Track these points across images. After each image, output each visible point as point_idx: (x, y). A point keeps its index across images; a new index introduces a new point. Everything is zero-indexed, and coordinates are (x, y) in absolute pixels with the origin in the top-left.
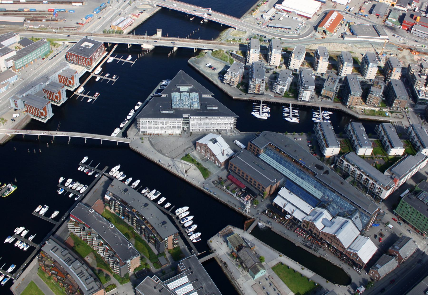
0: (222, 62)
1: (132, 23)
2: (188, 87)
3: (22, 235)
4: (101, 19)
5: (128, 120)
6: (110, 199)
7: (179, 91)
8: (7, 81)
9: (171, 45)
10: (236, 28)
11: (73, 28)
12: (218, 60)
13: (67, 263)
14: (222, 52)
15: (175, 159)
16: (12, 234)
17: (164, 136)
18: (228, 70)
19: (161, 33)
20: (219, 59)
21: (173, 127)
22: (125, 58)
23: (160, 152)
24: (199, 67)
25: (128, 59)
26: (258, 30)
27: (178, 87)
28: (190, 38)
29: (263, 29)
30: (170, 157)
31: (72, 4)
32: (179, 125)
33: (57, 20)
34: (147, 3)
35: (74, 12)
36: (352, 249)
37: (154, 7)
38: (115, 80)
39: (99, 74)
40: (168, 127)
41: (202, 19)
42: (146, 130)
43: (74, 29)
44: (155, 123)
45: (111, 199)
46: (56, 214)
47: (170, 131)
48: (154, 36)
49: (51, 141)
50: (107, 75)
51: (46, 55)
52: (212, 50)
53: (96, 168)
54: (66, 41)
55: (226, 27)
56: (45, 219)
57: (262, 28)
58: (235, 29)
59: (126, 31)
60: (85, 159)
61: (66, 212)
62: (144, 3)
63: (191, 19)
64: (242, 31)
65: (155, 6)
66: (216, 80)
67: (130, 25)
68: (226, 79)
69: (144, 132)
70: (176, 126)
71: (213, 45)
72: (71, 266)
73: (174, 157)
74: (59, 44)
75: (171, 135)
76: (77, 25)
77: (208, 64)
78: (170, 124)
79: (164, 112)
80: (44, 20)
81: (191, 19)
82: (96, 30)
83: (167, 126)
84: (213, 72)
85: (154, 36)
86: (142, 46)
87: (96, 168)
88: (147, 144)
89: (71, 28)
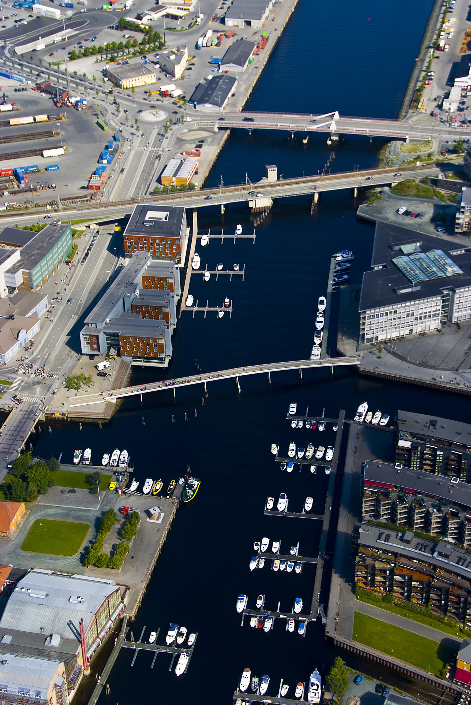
0: (424, 201)
1: (197, 169)
2: (414, 244)
3: (274, 550)
4: (125, 173)
5: (322, 329)
6: (411, 445)
7: (401, 253)
8: (33, 311)
9: (310, 191)
10: (407, 137)
11: (83, 197)
12: (414, 200)
13: (424, 552)
14: (413, 184)
15: (460, 371)
16: (254, 554)
17: (411, 339)
18: (463, 204)
19: (275, 173)
20: (413, 197)
21: (425, 317)
22: (233, 231)
23: (423, 365)
24: (386, 219)
25: (239, 232)
26: (450, 133)
27: (397, 248)
28: (327, 173)
29: (458, 130)
30: (448, 370)
31: (42, 155)
32: (436, 311)
33: (35, 190)
34: (196, 127)
35: (58, 168)
36: (282, 687)
37: (215, 133)
38: (243, 273)
39: (202, 267)
40: (416, 319)
41: (328, 135)
42: (376, 335)
43: (85, 199)
44: (393, 316)
45: (414, 446)
46: (309, 504)
47: (418, 329)
48: (264, 181)
49: (201, 400)
50: (220, 267)
51: (71, 255)
52: (389, 185)
53: (323, 416)
54: (92, 222)
55: (387, 140)
56: (294, 515)
57: (455, 129)
58: (404, 140)
59: (198, 182)
60: (293, 409)
61: (326, 497)
62: (190, 128)
63: (305, 141)
64: (419, 141)
65: (216, 130)
66: (434, 233)
67: (196, 173)
68: (458, 224)
69: (371, 339)
70: (432, 313)
71: (388, 174)
72: (436, 554)
73: (456, 368)
74: (80, 231)
75: (423, 334)
76: (85, 192)
77: (400, 210)
78: (421, 311)
79: (403, 291)
80: (6, 193)
81: (305, 141)
82: (131, 194)
83: (414, 317)
84: (418, 220)
85: (262, 181)
86: (251, 205)
87: (323, 416)
88: (388, 358)
89: (77, 198)
